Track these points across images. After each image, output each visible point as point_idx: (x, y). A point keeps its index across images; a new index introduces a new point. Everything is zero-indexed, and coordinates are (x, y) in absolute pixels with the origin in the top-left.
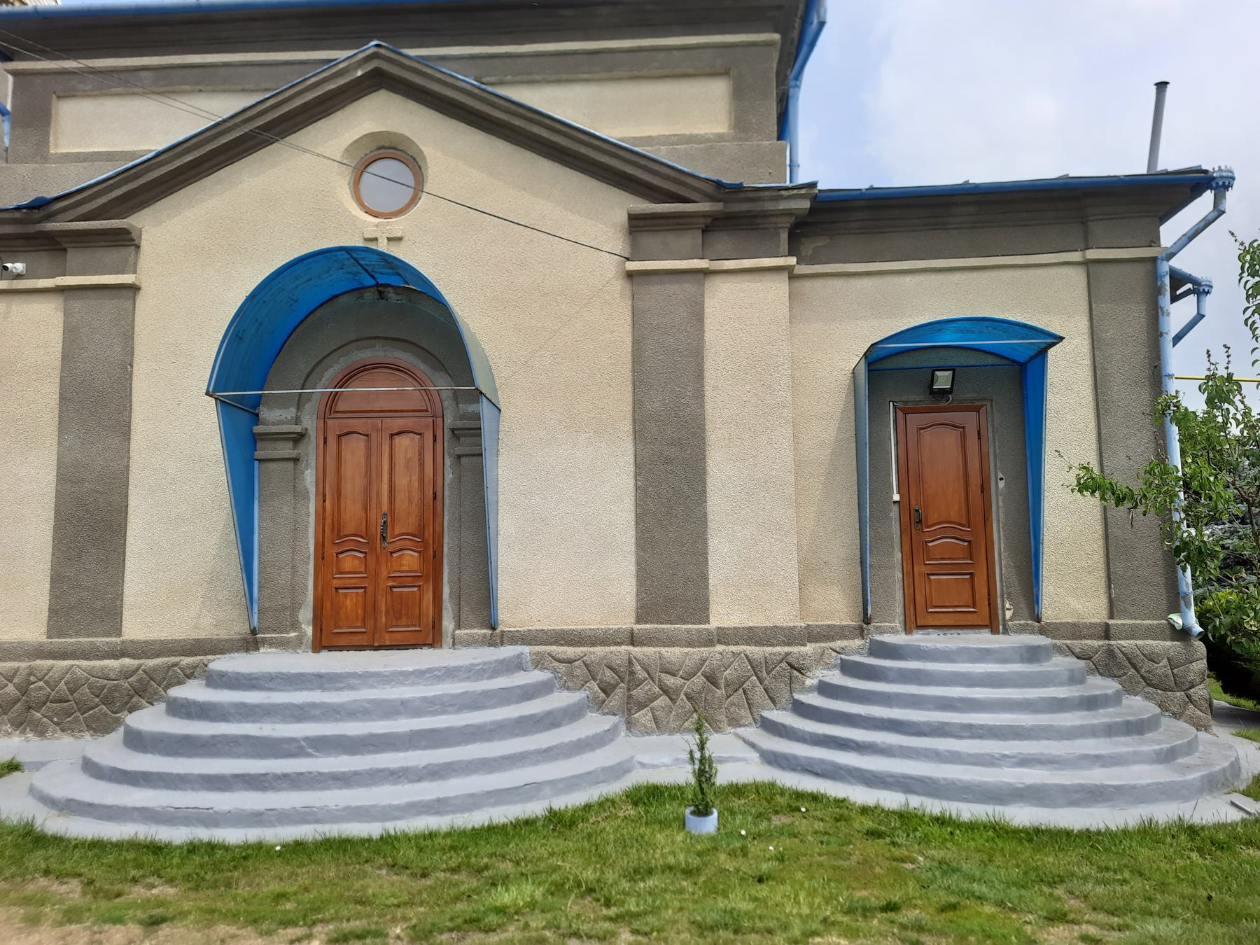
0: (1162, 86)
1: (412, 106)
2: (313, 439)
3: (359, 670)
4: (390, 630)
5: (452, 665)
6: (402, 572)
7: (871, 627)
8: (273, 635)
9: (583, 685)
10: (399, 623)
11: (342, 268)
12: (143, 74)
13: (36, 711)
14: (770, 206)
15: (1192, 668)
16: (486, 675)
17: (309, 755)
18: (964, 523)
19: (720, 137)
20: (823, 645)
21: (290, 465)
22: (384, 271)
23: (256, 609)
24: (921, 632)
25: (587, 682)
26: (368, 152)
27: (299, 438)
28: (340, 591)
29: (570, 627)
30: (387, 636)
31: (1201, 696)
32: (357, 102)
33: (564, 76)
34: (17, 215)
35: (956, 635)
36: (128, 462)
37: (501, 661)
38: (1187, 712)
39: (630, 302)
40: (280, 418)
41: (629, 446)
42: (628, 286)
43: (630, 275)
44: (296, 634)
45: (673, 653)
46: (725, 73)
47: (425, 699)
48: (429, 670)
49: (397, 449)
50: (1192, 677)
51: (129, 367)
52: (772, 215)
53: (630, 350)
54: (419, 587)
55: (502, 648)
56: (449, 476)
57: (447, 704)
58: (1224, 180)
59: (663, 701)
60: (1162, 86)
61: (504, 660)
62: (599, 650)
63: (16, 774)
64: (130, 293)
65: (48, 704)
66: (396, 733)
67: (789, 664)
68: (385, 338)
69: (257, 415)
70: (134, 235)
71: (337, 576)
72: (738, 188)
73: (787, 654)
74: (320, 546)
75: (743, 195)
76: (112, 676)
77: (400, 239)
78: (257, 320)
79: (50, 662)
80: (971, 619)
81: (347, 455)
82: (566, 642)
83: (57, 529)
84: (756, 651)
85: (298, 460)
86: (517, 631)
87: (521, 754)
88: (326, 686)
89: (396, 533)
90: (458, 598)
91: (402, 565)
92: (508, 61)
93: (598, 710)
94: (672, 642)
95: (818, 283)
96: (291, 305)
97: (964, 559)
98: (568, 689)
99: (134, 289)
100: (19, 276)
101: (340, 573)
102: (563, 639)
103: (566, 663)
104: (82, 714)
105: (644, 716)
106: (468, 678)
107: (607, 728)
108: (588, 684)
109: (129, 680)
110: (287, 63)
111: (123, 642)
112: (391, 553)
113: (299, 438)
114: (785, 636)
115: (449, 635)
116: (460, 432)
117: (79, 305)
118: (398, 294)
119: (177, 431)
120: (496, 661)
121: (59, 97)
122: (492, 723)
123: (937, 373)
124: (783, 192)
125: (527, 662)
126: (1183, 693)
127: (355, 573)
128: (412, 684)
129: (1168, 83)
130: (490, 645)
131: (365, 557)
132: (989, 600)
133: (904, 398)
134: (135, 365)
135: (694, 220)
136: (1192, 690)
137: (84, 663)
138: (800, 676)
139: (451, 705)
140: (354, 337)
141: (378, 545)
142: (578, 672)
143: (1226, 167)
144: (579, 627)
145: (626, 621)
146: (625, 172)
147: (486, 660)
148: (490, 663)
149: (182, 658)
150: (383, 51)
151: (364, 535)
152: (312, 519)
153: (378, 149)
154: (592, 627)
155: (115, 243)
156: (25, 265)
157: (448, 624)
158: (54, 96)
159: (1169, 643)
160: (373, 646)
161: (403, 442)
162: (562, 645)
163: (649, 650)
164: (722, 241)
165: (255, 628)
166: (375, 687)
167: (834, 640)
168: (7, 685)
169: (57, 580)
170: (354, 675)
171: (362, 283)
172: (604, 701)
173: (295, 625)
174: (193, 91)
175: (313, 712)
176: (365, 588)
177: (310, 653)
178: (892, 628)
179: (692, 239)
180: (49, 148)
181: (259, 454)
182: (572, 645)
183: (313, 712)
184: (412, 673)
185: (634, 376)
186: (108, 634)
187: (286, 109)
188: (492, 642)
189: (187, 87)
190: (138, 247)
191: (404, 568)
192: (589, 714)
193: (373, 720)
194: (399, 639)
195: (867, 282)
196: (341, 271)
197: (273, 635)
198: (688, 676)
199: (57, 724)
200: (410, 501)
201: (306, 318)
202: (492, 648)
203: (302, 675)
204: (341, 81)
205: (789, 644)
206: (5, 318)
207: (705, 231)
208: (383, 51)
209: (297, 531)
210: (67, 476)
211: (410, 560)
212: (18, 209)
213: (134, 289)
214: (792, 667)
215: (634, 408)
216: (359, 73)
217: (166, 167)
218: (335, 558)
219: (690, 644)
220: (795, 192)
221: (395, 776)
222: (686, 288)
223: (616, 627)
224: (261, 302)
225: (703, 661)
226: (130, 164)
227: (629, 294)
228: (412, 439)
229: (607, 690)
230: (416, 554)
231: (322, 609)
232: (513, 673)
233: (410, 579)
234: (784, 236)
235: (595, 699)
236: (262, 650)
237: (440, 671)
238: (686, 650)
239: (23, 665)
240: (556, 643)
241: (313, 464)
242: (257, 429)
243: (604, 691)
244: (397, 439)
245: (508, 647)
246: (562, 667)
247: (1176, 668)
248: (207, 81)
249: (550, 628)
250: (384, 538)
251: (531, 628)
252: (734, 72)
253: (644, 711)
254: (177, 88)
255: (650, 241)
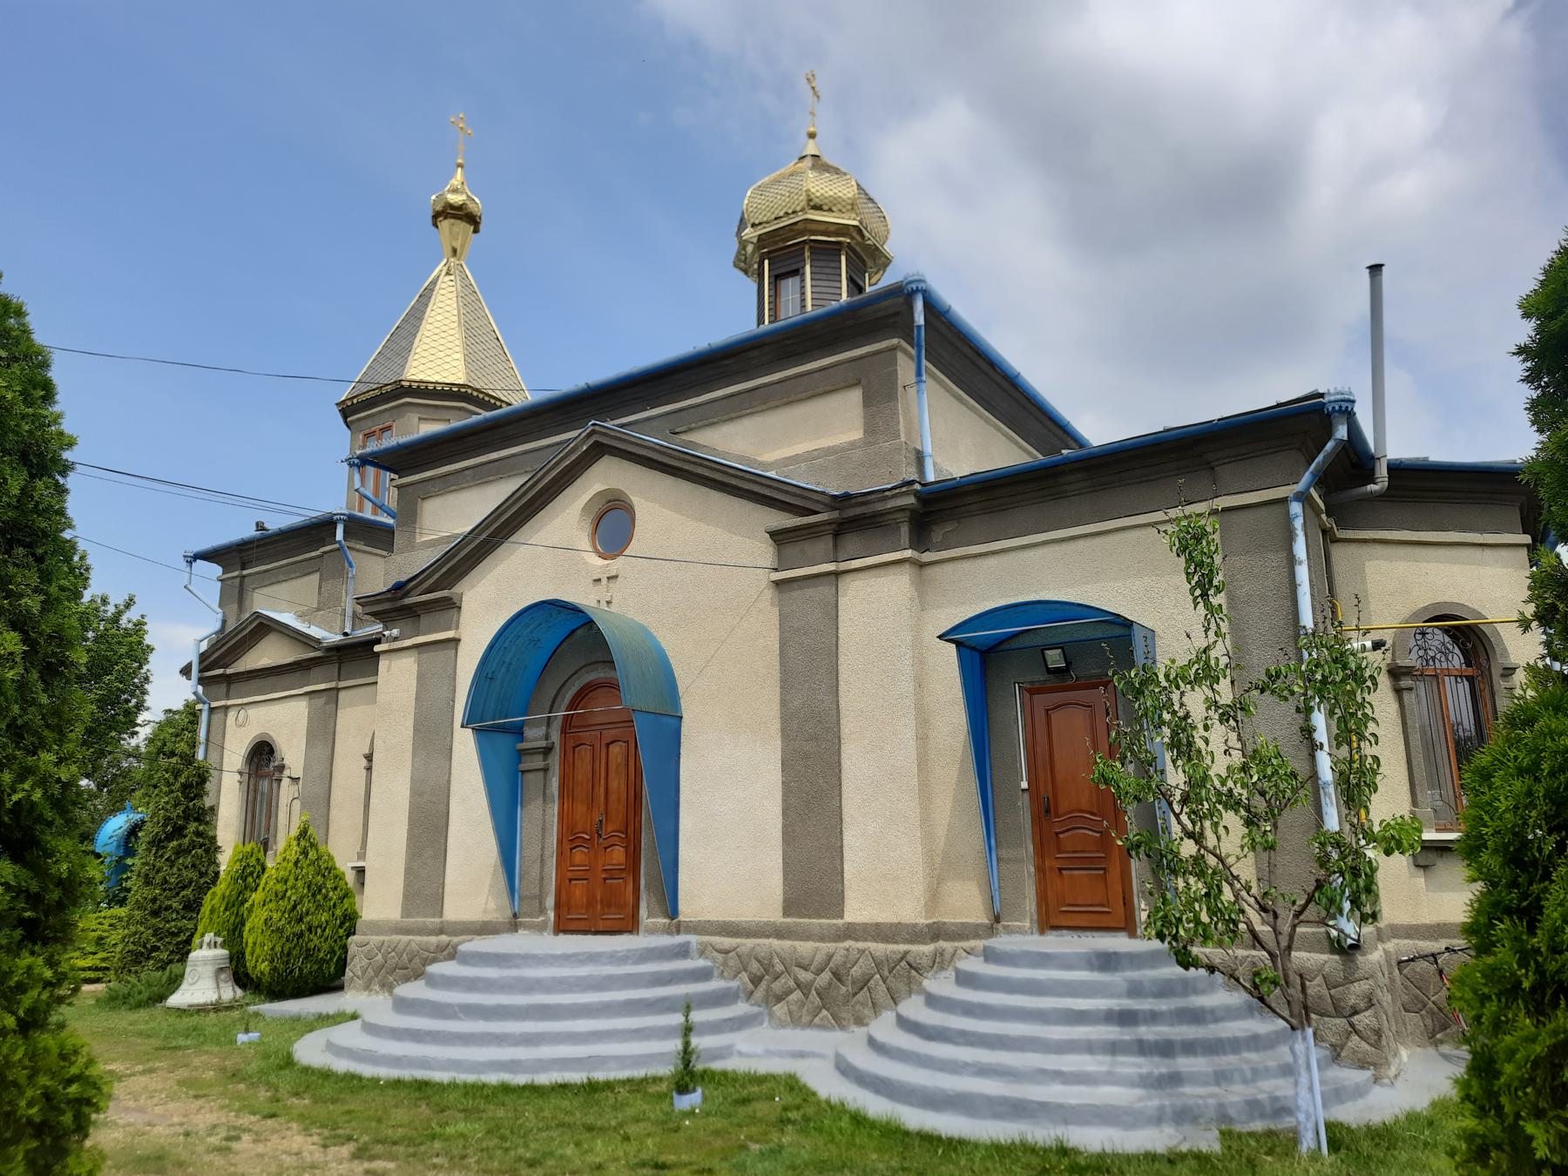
0: (1376, 269)
1: (625, 463)
2: (558, 750)
3: (521, 952)
7: (999, 926)
12: (467, 472)
14: (879, 507)
15: (1352, 989)
18: (1095, 811)
19: (853, 445)
20: (956, 944)
21: (541, 774)
23: (516, 897)
24: (1054, 933)
27: (547, 751)
30: (601, 922)
31: (1367, 1025)
33: (733, 415)
34: (389, 595)
35: (1076, 938)
38: (1350, 1044)
43: (777, 583)
45: (805, 948)
46: (857, 383)
47: (554, 979)
48: (575, 955)
50: (1352, 1001)
52: (888, 513)
58: (1333, 405)
59: (797, 995)
60: (1376, 269)
62: (749, 943)
67: (908, 963)
72: (847, 497)
73: (906, 953)
75: (854, 501)
76: (432, 949)
77: (616, 577)
80: (1105, 920)
83: (410, 831)
84: (879, 948)
92: (692, 410)
94: (806, 936)
95: (948, 567)
97: (1098, 851)
100: (396, 639)
101: (573, 866)
105: (780, 1009)
106: (610, 963)
110: (549, 446)
114: (908, 934)
117: (428, 656)
121: (423, 499)
123: (1047, 652)
124: (887, 493)
126: (1344, 1020)
129: (1381, 265)
132: (1124, 899)
133: (1028, 678)
135: (822, 528)
136: (1356, 1017)
137: (418, 938)
138: (918, 976)
140: (583, 663)
143: (1336, 389)
145: (773, 913)
159: (1325, 957)
163: (787, 944)
164: (851, 542)
167: (968, 939)
169: (409, 871)
170: (518, 956)
174: (497, 479)
178: (1019, 927)
179: (825, 544)
180: (415, 539)
181: (523, 767)
186: (434, 916)
187: (540, 486)
188: (668, 931)
189: (491, 478)
195: (992, 562)
198: (819, 971)
201: (555, 651)
204: (573, 457)
205: (911, 942)
207: (837, 535)
208: (597, 428)
211: (618, 855)
212: (389, 591)
213: (456, 641)
214: (911, 966)
216: (585, 448)
219: (822, 939)
220: (897, 491)
222: (822, 591)
225: (830, 957)
226: (453, 545)
229: (756, 981)
234: (905, 530)
236: (520, 932)
238: (817, 944)
239: (386, 938)
240: (719, 934)
242: (521, 746)
246: (720, 957)
247: (1335, 987)
248: (482, 476)
250: (600, 836)
252: (864, 382)
253: (780, 1005)
254: (486, 479)
255: (792, 551)
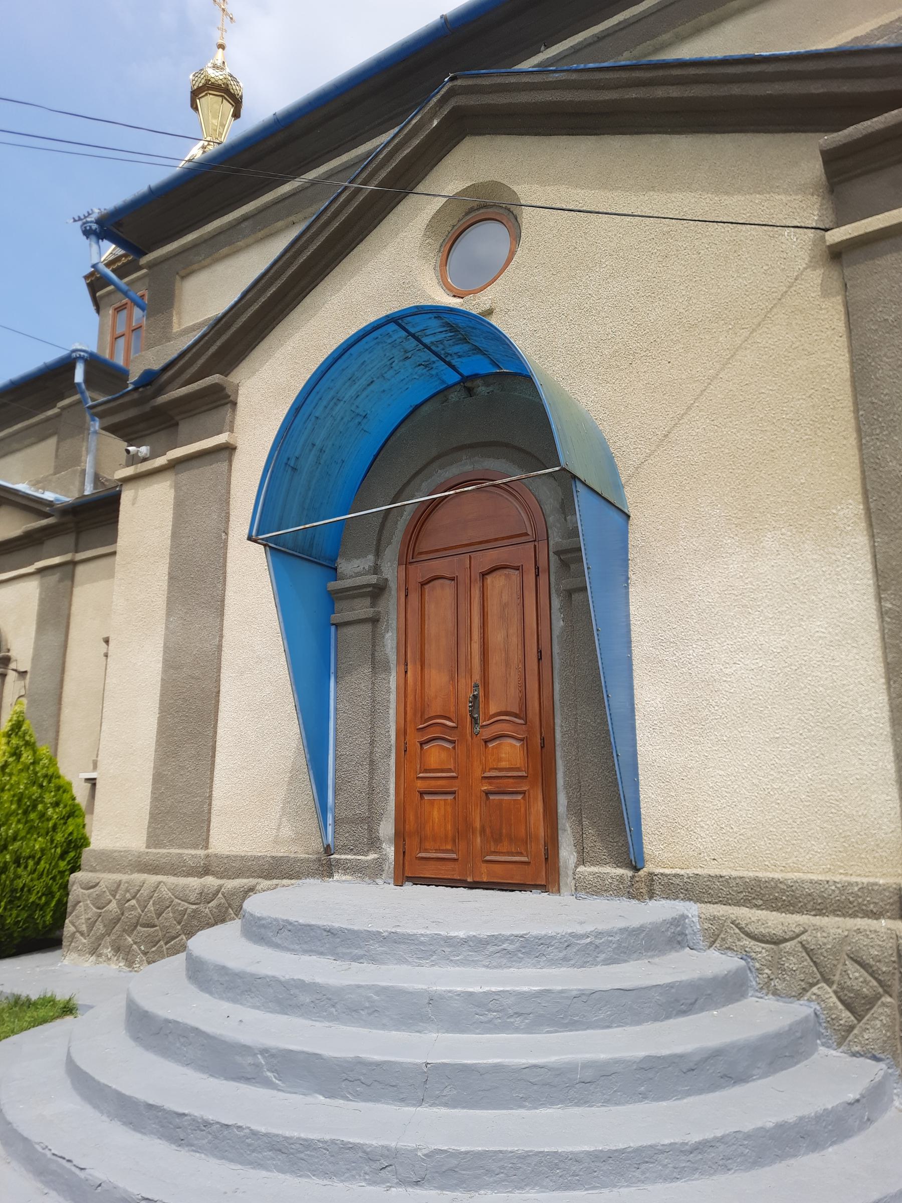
2: (394, 592)
4: (488, 858)
5: (535, 932)
6: (500, 770)
8: (349, 857)
9: (805, 990)
10: (500, 848)
11: (407, 358)
13: (129, 935)
16: (602, 956)
17: (267, 1084)
21: (368, 627)
22: (456, 349)
23: (330, 820)
25: (812, 985)
26: (455, 221)
27: (377, 592)
28: (426, 797)
29: (771, 875)
30: (484, 868)
32: (437, 167)
36: (220, 641)
37: (634, 930)
39: (839, 299)
40: (358, 570)
41: (862, 540)
42: (835, 274)
44: (376, 856)
49: (489, 592)
51: (223, 534)
53: (847, 375)
54: (523, 793)
55: (652, 903)
56: (559, 624)
57: (511, 1012)
61: (641, 929)
63: (69, 1019)
64: (226, 454)
65: (139, 928)
66: (400, 1064)
68: (472, 446)
69: (335, 569)
70: (229, 391)
71: (421, 775)
74: (402, 733)
78: (314, 445)
79: (144, 876)
81: (431, 608)
82: (765, 902)
83: (162, 720)
85: (378, 621)
86: (676, 875)
87: (638, 1151)
88: (340, 950)
89: (492, 712)
90: (577, 811)
91: (500, 760)
93: (840, 1045)
96: (359, 423)
98: (775, 993)
99: (228, 450)
100: (145, 459)
101: (426, 771)
102: (760, 896)
103: (767, 942)
104: (166, 944)
107: (851, 1096)
108: (815, 989)
109: (210, 905)
111: (208, 856)
112: (486, 742)
113: (377, 592)
115: (570, 873)
116: (569, 555)
118: (488, 386)
119: (264, 601)
120: (622, 931)
122: (586, 1065)
125: (695, 933)
127: (442, 771)
128: (465, 962)
130: (631, 896)
131: (454, 748)
134: (230, 532)
137: (171, 880)
139: (519, 1014)
141: (468, 731)
142: (791, 963)
144: (790, 876)
146: (812, 94)
147: (601, 927)
148: (610, 934)
149: (260, 880)
150: (459, 82)
151: (453, 716)
152: (393, 697)
153: (467, 214)
154: (815, 877)
155: (215, 404)
156: (149, 447)
157: (567, 854)
158: (178, 277)
160: (465, 881)
161: (496, 582)
162: (758, 907)
165: (328, 846)
166: (406, 962)
168: (111, 901)
169: (158, 778)
171: (443, 382)
172: (852, 1028)
173: (374, 843)
175: (306, 999)
176: (453, 793)
177: (392, 886)
181: (336, 618)
182: (778, 909)
183: (306, 999)
184: (465, 941)
185: (857, 418)
186: (195, 846)
188: (633, 894)
190: (235, 404)
191: (504, 764)
192: (822, 1050)
193: (384, 1027)
194: (499, 873)
196: (407, 362)
197: (349, 857)
199: (145, 953)
200: (507, 665)
202: (634, 902)
203: (310, 927)
206: (133, 504)
209: (374, 713)
210: (171, 664)
215: (863, 472)
216: (435, 123)
217: (252, 308)
218: (419, 751)
221: (377, 1165)
223: (865, 880)
224: (313, 419)
227: (837, 285)
228: (508, 576)
230: (518, 744)
231: (404, 821)
232: (662, 952)
233: (511, 780)
235: (832, 1021)
236: (336, 877)
237: (512, 942)
241: (394, 625)
242: (333, 585)
243: (848, 1006)
244: (489, 579)
245: (663, 902)
246: (761, 951)
249: (734, 874)
250: (475, 721)
251: (699, 871)
